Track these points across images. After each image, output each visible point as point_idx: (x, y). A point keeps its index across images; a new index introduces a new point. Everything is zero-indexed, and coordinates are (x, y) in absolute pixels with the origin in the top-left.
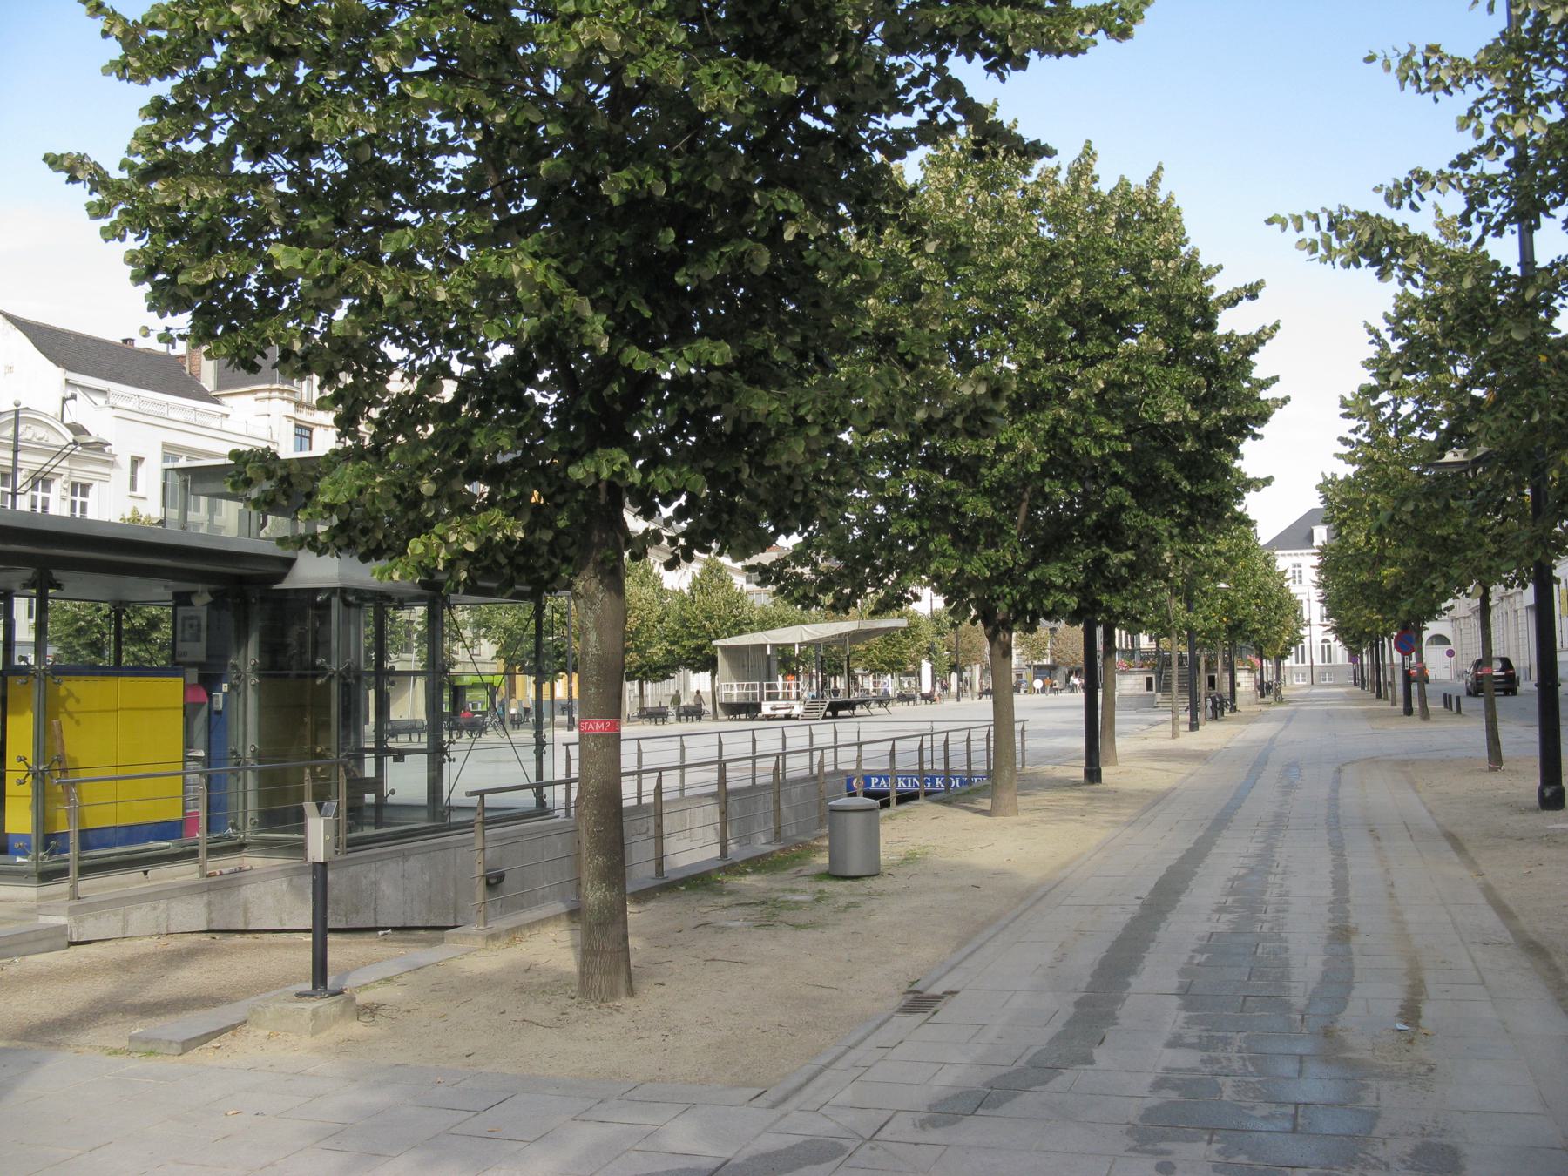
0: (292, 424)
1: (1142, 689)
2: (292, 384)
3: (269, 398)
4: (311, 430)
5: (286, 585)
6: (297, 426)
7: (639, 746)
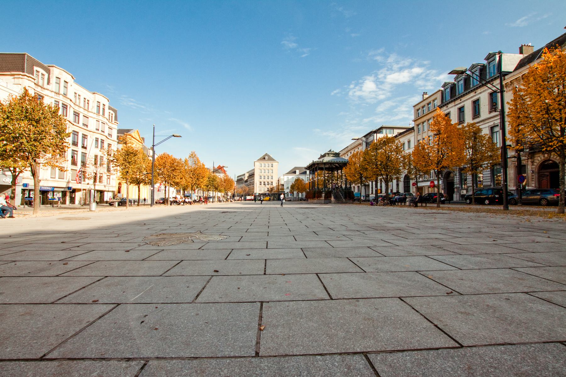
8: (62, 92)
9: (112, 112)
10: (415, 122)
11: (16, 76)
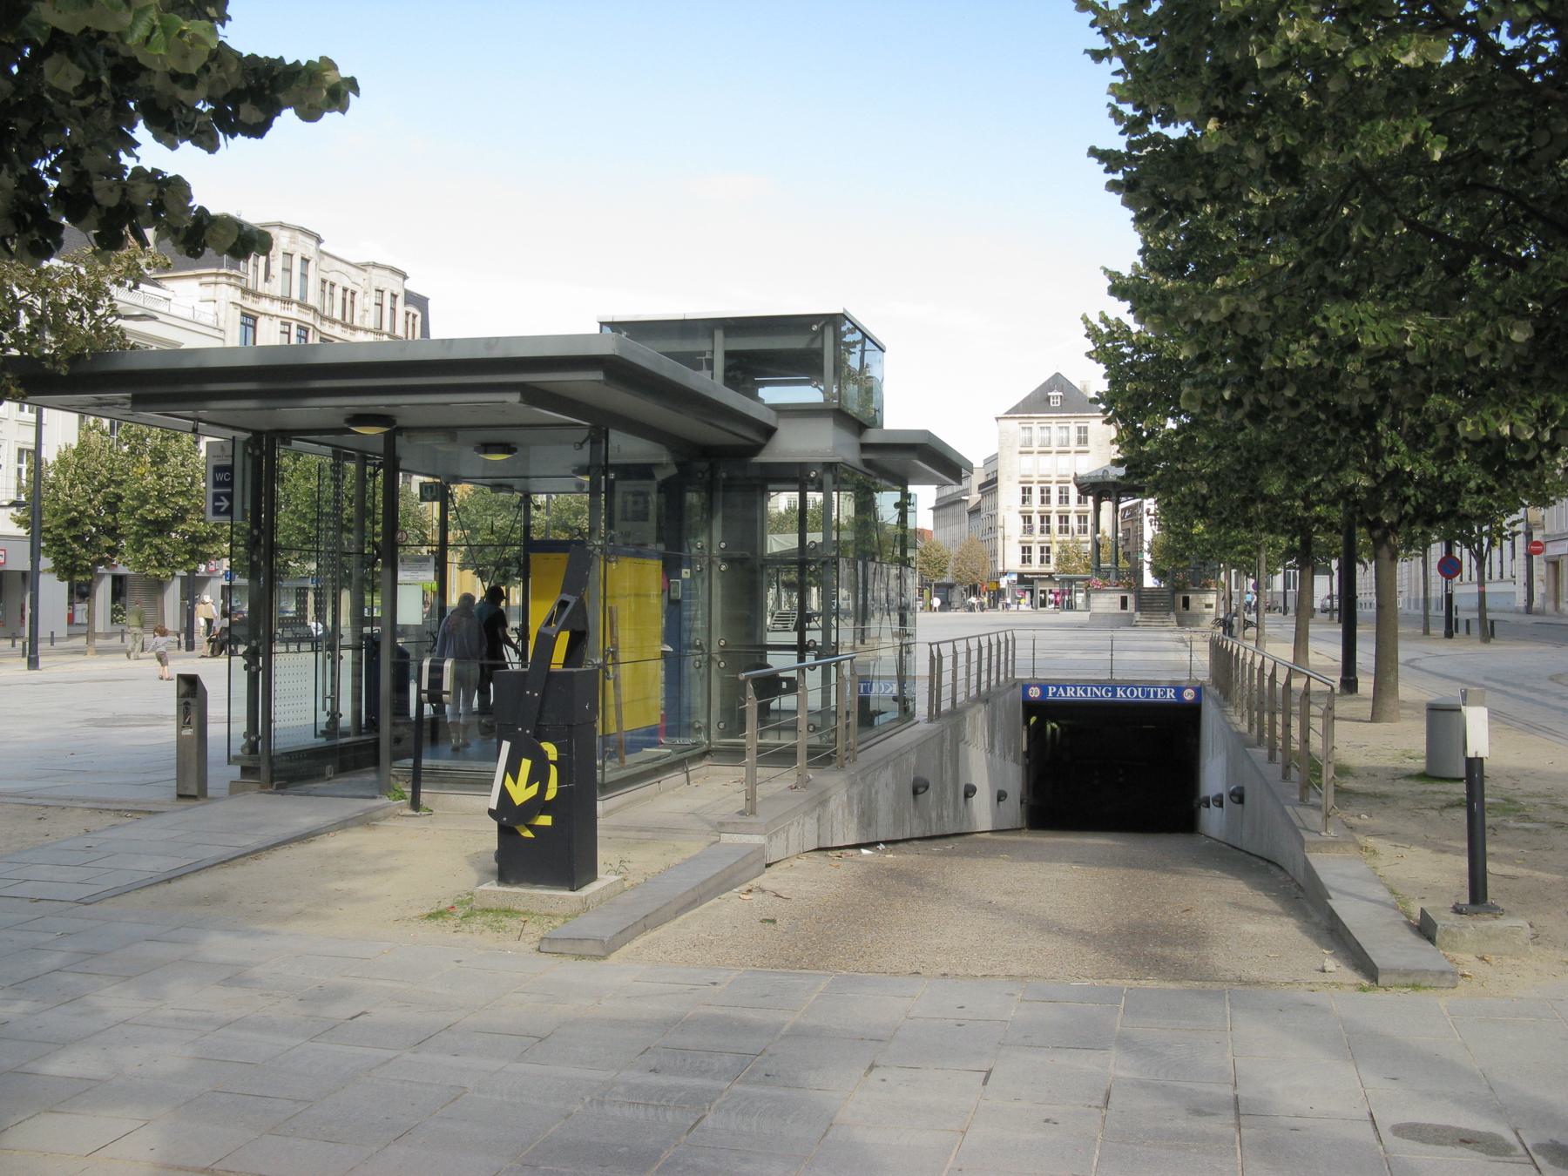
0: (238, 312)
1: (1117, 608)
2: (238, 269)
3: (216, 283)
4: (255, 319)
5: (762, 458)
6: (243, 314)
7: (954, 647)
8: (296, 296)
9: (413, 310)
10: (941, 512)
11: (205, 280)
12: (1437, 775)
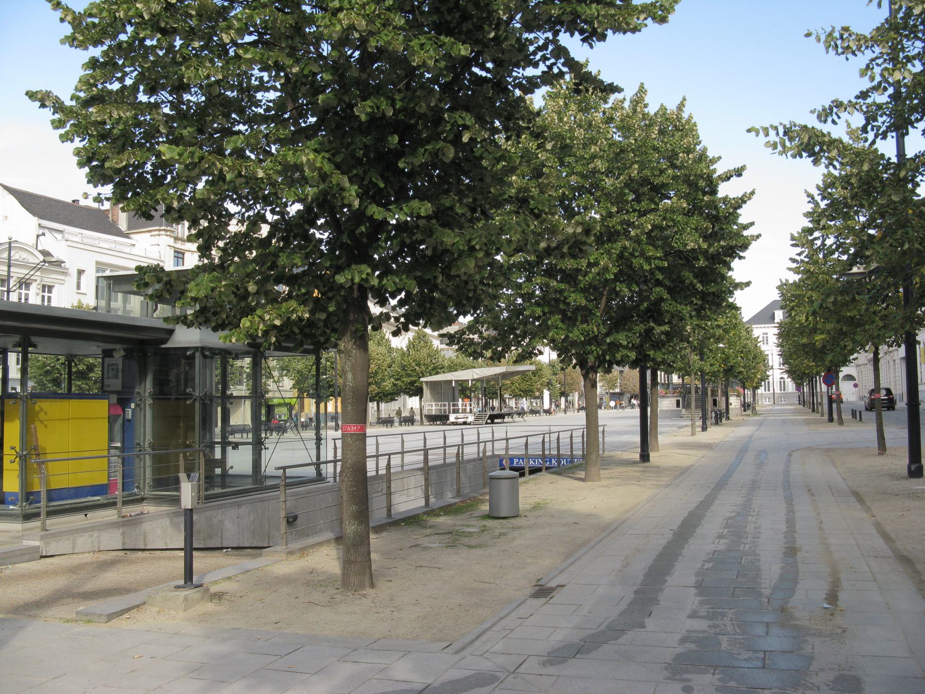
0: (172, 250)
1: (674, 407)
2: (172, 227)
3: (159, 235)
4: (183, 254)
5: (169, 345)
6: (175, 251)
7: (377, 440)
12: (498, 516)
